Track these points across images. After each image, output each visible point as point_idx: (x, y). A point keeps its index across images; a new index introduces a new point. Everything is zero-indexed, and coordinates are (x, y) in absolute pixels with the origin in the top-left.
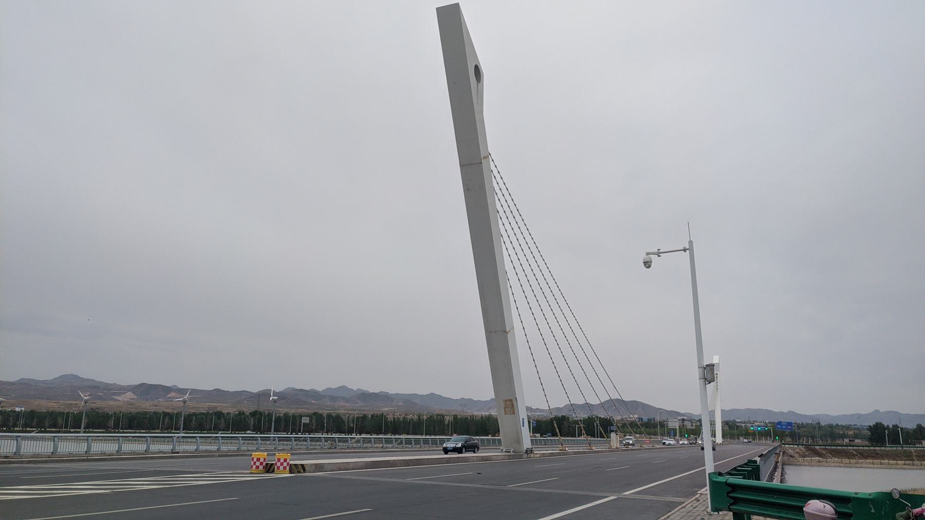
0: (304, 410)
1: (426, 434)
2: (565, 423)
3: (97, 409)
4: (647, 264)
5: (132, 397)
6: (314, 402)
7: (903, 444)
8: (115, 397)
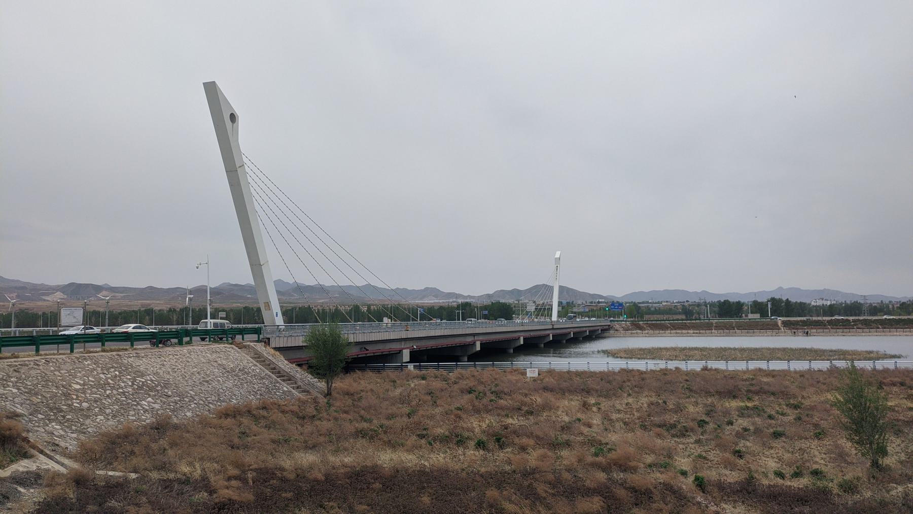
0: (239, 305)
1: (186, 325)
2: (468, 308)
3: (26, 309)
4: (197, 268)
5: (62, 297)
6: (250, 296)
7: (771, 317)
8: (44, 297)
